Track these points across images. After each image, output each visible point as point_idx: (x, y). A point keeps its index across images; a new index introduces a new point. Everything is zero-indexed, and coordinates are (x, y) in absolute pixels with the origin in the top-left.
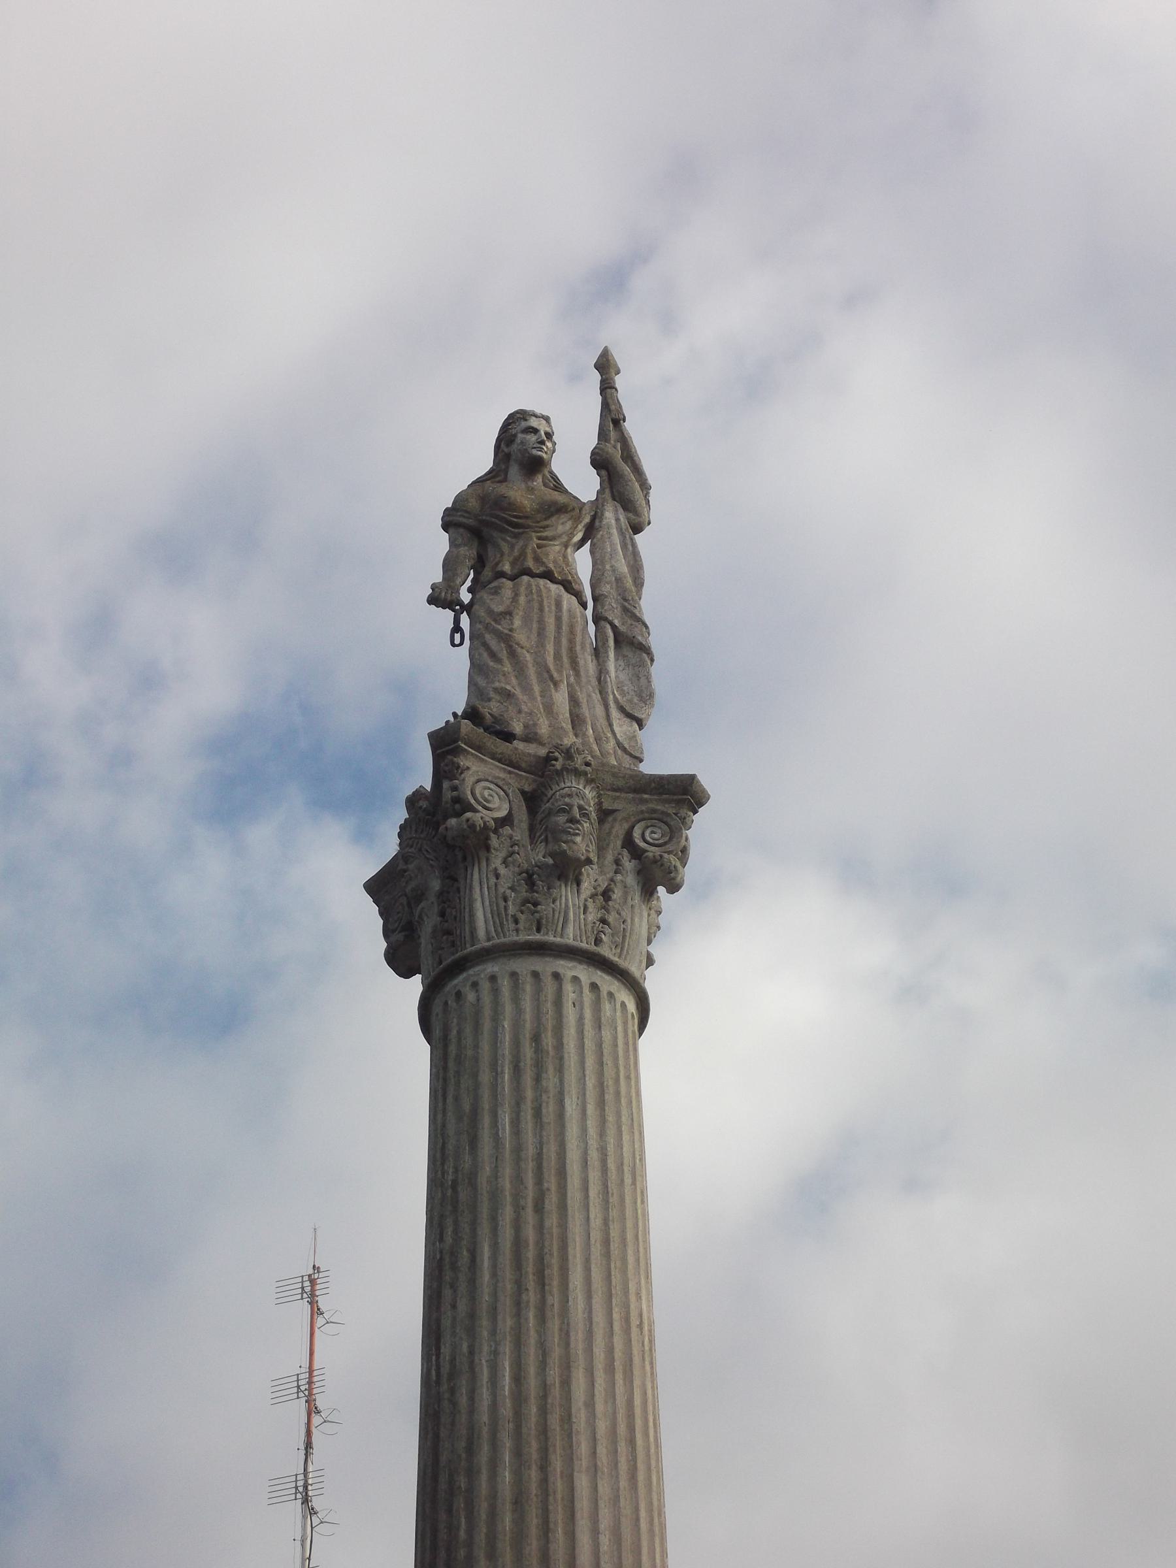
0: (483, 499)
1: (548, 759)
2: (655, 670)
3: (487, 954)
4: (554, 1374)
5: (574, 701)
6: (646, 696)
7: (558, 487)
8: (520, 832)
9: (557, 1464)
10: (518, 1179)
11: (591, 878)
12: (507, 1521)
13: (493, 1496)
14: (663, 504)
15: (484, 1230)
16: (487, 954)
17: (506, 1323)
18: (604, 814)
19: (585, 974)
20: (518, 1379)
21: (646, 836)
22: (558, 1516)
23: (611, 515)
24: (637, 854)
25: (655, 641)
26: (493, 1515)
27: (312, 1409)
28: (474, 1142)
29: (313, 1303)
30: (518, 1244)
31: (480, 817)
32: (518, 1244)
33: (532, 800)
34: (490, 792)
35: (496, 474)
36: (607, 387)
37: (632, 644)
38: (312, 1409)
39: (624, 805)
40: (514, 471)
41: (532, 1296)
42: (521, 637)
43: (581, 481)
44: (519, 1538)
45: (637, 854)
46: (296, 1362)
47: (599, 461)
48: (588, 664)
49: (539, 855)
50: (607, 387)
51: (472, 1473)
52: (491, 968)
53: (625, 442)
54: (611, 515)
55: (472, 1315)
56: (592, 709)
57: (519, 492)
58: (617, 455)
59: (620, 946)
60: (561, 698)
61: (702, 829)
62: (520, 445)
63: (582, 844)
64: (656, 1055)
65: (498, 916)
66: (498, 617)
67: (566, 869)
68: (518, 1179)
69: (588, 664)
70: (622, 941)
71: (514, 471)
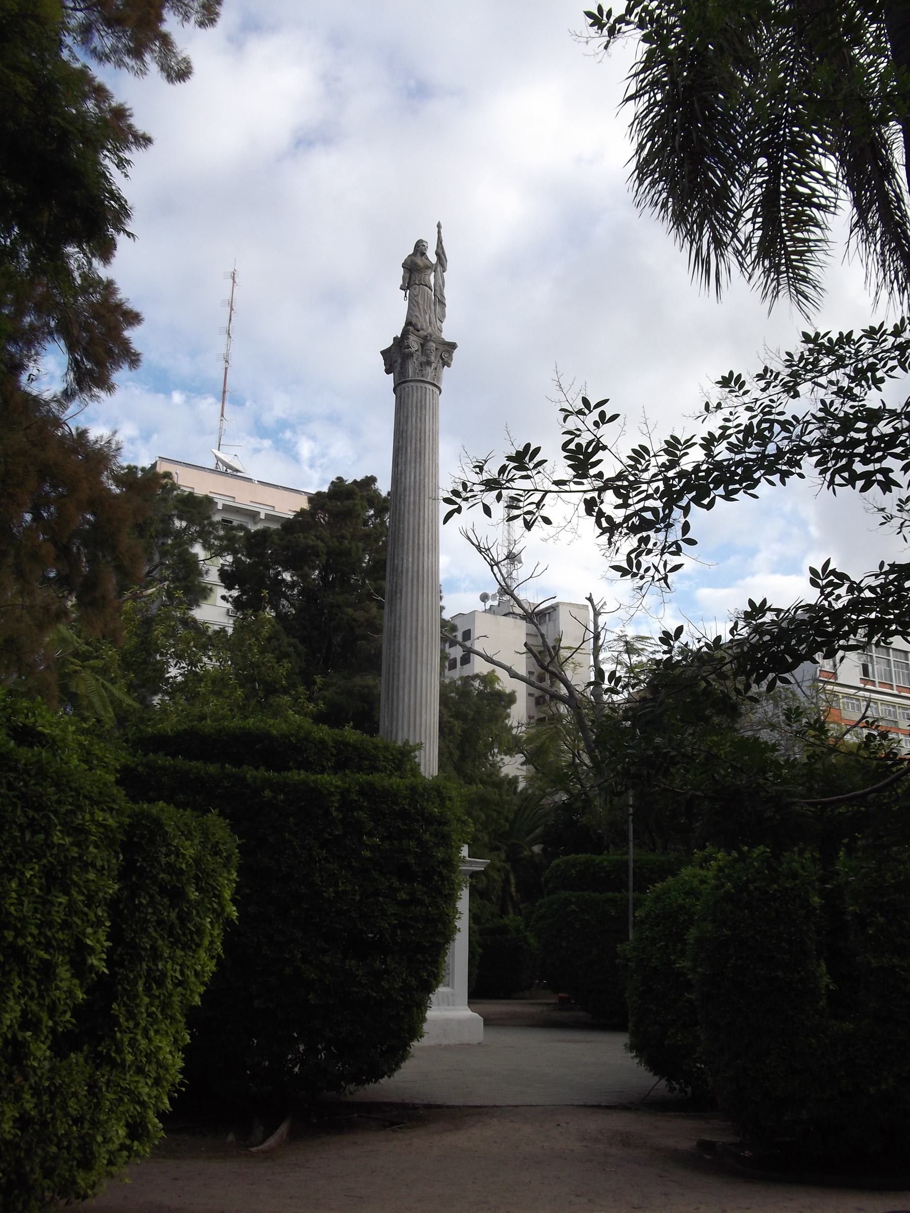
0: (412, 261)
1: (426, 336)
2: (447, 309)
3: (411, 381)
4: (422, 477)
5: (430, 318)
6: (444, 316)
7: (427, 259)
8: (419, 353)
9: (422, 496)
10: (416, 433)
11: (434, 365)
12: (412, 507)
13: (409, 502)
14: (449, 265)
15: (409, 444)
16: (411, 381)
17: (413, 465)
18: (437, 349)
19: (430, 387)
20: (415, 477)
21: (445, 355)
22: (422, 508)
23: (439, 269)
24: (442, 359)
25: (447, 302)
26: (409, 506)
27: (232, 309)
28: (407, 422)
29: (234, 279)
30: (416, 448)
31: (413, 350)
32: (416, 448)
33: (422, 345)
34: (414, 344)
35: (414, 254)
36: (439, 232)
37: (441, 302)
38: (232, 309)
39: (441, 347)
40: (418, 254)
41: (418, 460)
42: (420, 302)
43: (433, 259)
44: (414, 511)
45: (442, 359)
46: (228, 297)
47: (437, 254)
48: (433, 307)
49: (424, 359)
50: (439, 232)
51: (405, 496)
52: (412, 384)
53: (442, 248)
54: (439, 269)
55: (406, 461)
56: (433, 320)
57: (419, 261)
58: (441, 252)
59: (438, 381)
60: (427, 317)
61: (456, 353)
62: (420, 249)
63: (433, 358)
64: (442, 399)
65: (414, 372)
66: (416, 296)
67: (429, 363)
68: (416, 433)
69: (433, 307)
70: (439, 379)
71: (418, 254)
